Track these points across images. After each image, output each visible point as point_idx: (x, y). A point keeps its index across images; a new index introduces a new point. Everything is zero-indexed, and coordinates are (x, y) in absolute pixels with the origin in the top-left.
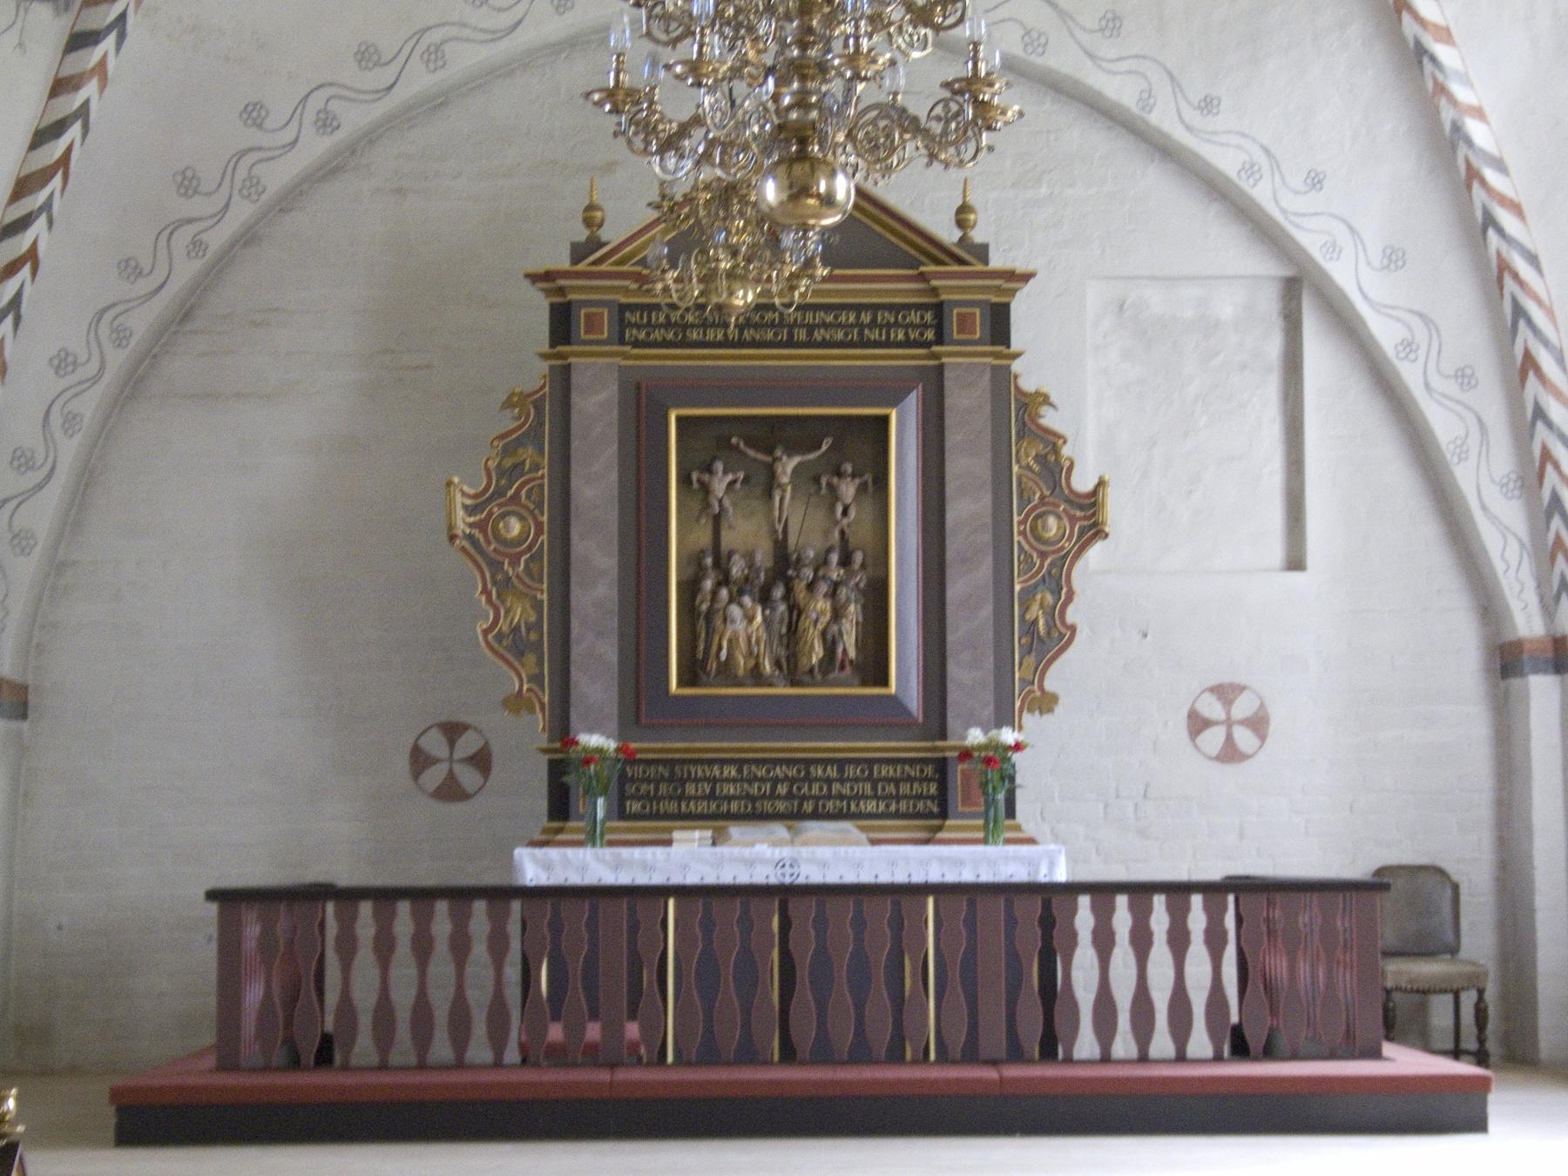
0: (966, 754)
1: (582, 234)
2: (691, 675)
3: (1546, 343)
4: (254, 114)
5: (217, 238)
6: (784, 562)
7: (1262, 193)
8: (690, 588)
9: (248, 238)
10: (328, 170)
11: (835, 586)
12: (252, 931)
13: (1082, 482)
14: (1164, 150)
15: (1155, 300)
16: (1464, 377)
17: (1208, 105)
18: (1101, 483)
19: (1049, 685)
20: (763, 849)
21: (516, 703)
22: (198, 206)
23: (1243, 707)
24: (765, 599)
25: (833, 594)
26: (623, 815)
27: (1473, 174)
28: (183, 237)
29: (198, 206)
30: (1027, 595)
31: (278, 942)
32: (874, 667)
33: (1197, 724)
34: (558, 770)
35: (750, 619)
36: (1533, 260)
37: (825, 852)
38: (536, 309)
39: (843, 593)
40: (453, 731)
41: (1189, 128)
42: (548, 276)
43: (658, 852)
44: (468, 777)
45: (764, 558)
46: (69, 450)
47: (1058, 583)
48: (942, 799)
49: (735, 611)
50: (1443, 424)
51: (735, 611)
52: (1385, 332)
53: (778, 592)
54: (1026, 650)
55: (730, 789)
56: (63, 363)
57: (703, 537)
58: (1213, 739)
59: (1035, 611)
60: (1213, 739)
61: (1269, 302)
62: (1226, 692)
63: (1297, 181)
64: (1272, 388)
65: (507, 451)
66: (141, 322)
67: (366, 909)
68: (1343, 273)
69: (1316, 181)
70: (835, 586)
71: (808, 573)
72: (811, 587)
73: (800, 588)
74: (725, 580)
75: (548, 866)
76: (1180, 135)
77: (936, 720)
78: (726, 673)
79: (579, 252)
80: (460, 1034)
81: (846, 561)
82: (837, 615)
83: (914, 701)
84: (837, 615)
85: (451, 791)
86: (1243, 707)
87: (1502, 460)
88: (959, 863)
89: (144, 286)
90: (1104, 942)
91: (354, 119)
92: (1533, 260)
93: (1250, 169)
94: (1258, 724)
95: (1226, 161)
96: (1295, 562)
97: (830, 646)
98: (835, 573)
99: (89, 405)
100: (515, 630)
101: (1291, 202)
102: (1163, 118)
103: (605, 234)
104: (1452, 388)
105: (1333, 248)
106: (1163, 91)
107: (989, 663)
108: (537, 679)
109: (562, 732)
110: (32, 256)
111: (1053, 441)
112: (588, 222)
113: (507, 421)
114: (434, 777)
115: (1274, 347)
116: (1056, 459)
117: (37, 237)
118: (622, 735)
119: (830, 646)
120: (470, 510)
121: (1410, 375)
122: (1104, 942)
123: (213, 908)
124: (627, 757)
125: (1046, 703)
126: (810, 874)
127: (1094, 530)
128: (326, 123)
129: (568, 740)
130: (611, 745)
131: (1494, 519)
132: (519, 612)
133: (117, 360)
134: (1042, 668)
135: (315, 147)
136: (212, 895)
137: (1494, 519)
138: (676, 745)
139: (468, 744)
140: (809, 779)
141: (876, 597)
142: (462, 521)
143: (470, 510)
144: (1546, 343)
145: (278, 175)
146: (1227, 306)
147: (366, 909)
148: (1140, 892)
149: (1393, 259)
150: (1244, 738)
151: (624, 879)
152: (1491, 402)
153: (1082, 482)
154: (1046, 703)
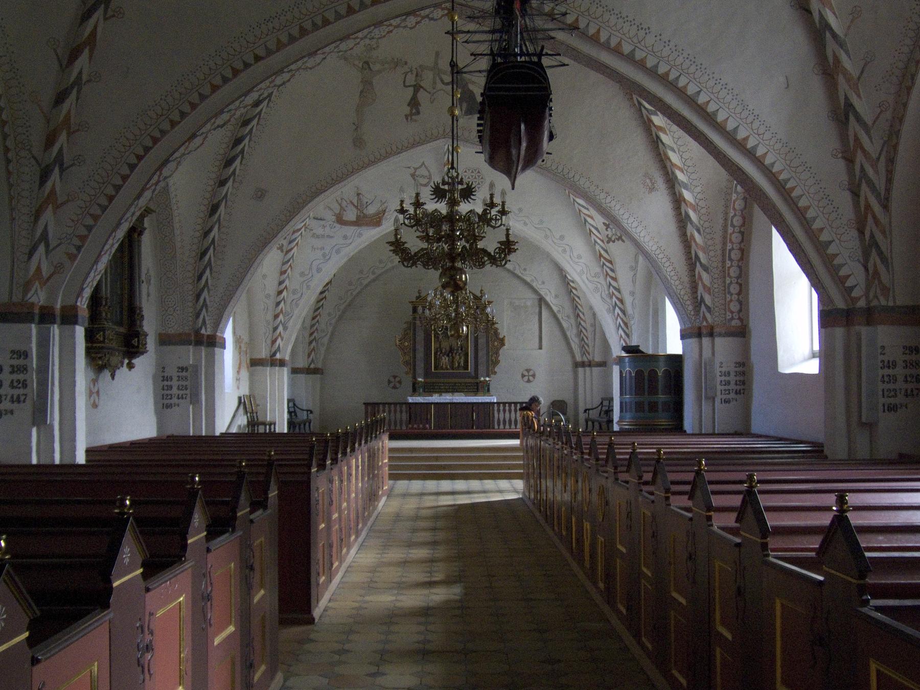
0: (481, 382)
1: (418, 295)
2: (436, 368)
3: (580, 311)
4: (361, 272)
5: (354, 293)
6: (451, 350)
7: (534, 285)
8: (436, 354)
9: (360, 293)
10: (374, 280)
11: (460, 354)
12: (369, 408)
13: (501, 336)
14: (518, 277)
15: (517, 302)
16: (568, 317)
17: (525, 270)
18: (504, 337)
19: (496, 370)
20: (448, 397)
21: (407, 373)
22: (353, 287)
23: (531, 373)
24: (448, 356)
25: (459, 355)
26: (424, 392)
27: (568, 283)
28: (349, 293)
29: (353, 287)
30: (492, 356)
31: (644, 379)
32: (466, 368)
33: (523, 376)
34: (414, 385)
35: (445, 359)
36: (579, 298)
37: (457, 398)
38: (410, 307)
39: (461, 355)
40: (395, 377)
41: (522, 274)
42: (412, 302)
43: (430, 398)
44: (398, 385)
45: (448, 348)
46: (330, 329)
47: (497, 353)
48: (478, 389)
49: (443, 358)
50: (565, 325)
51: (443, 358)
52: (555, 309)
53: (450, 355)
54: (492, 364)
55: (442, 387)
56: (329, 314)
57: (438, 346)
58: (526, 379)
59: (493, 358)
60: (526, 379)
61: (536, 303)
62: (528, 371)
63: (540, 283)
64: (537, 317)
65: (405, 331)
66: (342, 307)
67: (398, 406)
68: (548, 298)
69: (543, 283)
70: (460, 354)
71: (455, 351)
72: (456, 354)
73: (454, 355)
74: (441, 352)
75: (413, 400)
76: (520, 275)
77: (477, 377)
78: (442, 368)
79: (417, 298)
80: (401, 425)
81: (461, 349)
82: (460, 358)
83: (473, 374)
84: (460, 358)
85: (395, 387)
86: (531, 373)
87: (575, 331)
88: (478, 399)
89: (343, 301)
90: (499, 411)
91: (378, 272)
92: (579, 298)
93: (532, 280)
94: (534, 376)
95: (528, 279)
96: (540, 348)
97: (459, 363)
98: (460, 351)
99: (334, 321)
100: (407, 361)
101: (539, 286)
102: (517, 272)
103: (421, 295)
104: (566, 318)
105: (546, 294)
106: (517, 267)
107: (485, 366)
108: (410, 369)
109: (414, 378)
110: (325, 297)
111: (496, 330)
112: (419, 293)
113: (405, 326)
114: (392, 385)
115: (537, 310)
116: (250, 667)
117: (82, 69)
118: (424, 378)
119: (459, 363)
120: (399, 341)
121: (559, 316)
122: (499, 411)
123: (364, 406)
124: (425, 383)
125: (495, 373)
126: (455, 401)
127: (503, 344)
128: (373, 273)
129: (416, 380)
130: (423, 380)
131: (574, 341)
132: (407, 358)
133: (338, 313)
134: (494, 367)
135: (372, 277)
136: (365, 404)
137: (574, 341)
138: (434, 380)
139: (398, 379)
140: (455, 386)
141: (467, 355)
142: (398, 343)
143: (399, 341)
144: (580, 311)
145: (365, 282)
146: (529, 303)
147: (398, 406)
148: (510, 404)
149: (556, 296)
150: (531, 378)
151: (425, 401)
152: (573, 321)
153: (501, 336)
154: (495, 373)
